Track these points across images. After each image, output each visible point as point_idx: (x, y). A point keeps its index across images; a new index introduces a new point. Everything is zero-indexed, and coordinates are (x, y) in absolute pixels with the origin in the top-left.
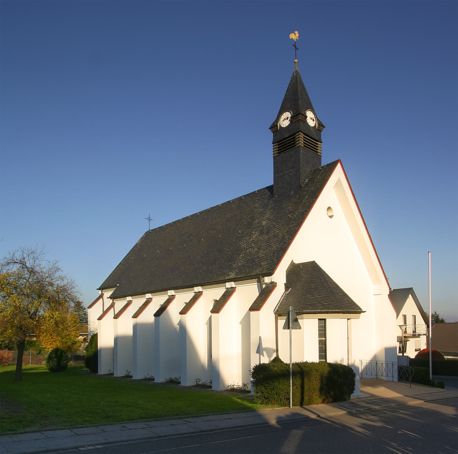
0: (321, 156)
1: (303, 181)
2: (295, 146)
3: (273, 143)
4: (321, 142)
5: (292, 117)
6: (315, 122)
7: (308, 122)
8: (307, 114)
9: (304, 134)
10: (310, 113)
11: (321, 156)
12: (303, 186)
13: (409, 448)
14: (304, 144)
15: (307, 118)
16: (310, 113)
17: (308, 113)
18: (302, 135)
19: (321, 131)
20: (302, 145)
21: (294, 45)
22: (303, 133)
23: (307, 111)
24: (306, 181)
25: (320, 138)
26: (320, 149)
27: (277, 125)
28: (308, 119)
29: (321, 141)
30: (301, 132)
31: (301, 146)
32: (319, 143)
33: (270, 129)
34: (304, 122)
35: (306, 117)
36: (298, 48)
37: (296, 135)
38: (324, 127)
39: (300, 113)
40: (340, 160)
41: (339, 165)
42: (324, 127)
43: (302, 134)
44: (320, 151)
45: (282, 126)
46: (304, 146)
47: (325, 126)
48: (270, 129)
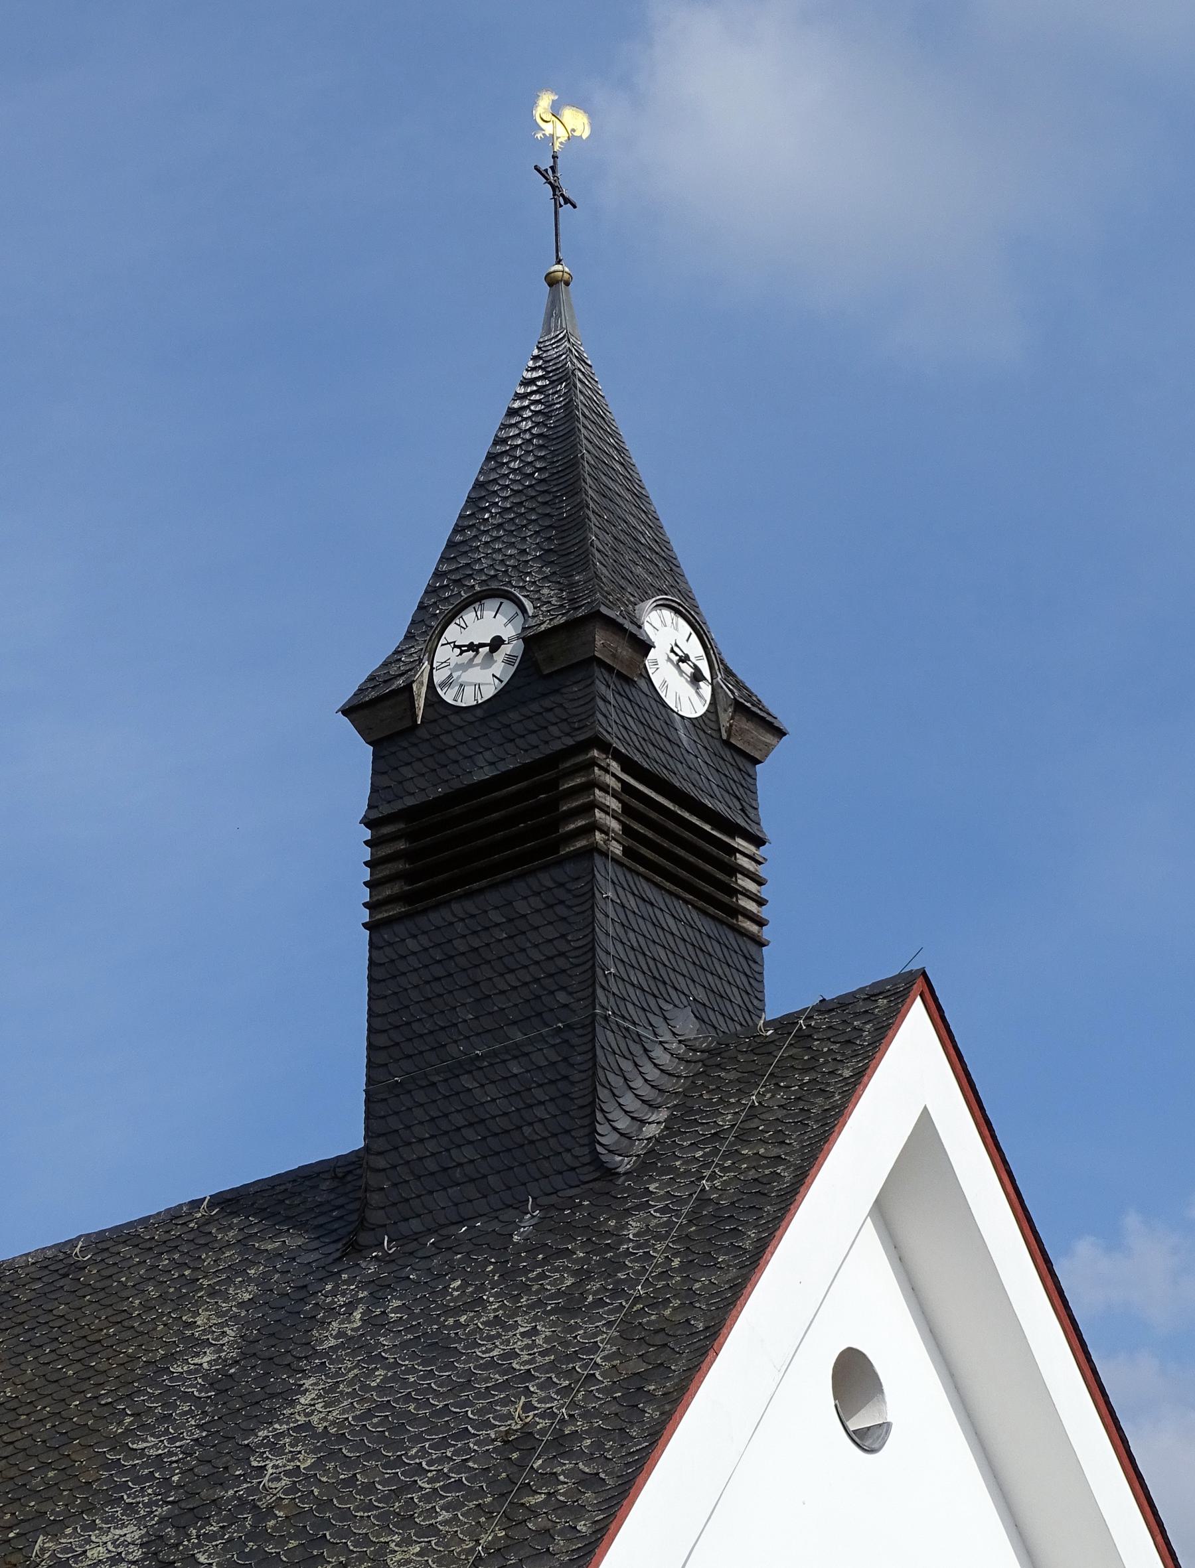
0: (761, 944)
1: (623, 1123)
2: (555, 847)
3: (368, 823)
4: (759, 842)
5: (532, 641)
6: (706, 689)
7: (657, 680)
8: (647, 627)
9: (628, 765)
10: (669, 622)
11: (761, 944)
12: (625, 1164)
13: (584, 823)
14: (630, 842)
15: (652, 654)
16: (669, 622)
17: (657, 624)
18: (612, 774)
19: (756, 762)
20: (616, 849)
21: (543, 174)
22: (618, 756)
23: (650, 603)
24: (651, 1130)
25: (748, 807)
26: (752, 886)
27: (408, 688)
28: (656, 663)
29: (752, 829)
30: (606, 747)
31: (605, 854)
32: (740, 843)
33: (347, 711)
34: (628, 680)
35: (645, 647)
36: (572, 198)
37: (561, 767)
38: (780, 733)
39: (597, 615)
40: (924, 974)
41: (917, 1017)
42: (785, 734)
43: (615, 766)
44: (752, 906)
45: (448, 696)
46: (627, 851)
47: (783, 722)
48: (347, 711)
